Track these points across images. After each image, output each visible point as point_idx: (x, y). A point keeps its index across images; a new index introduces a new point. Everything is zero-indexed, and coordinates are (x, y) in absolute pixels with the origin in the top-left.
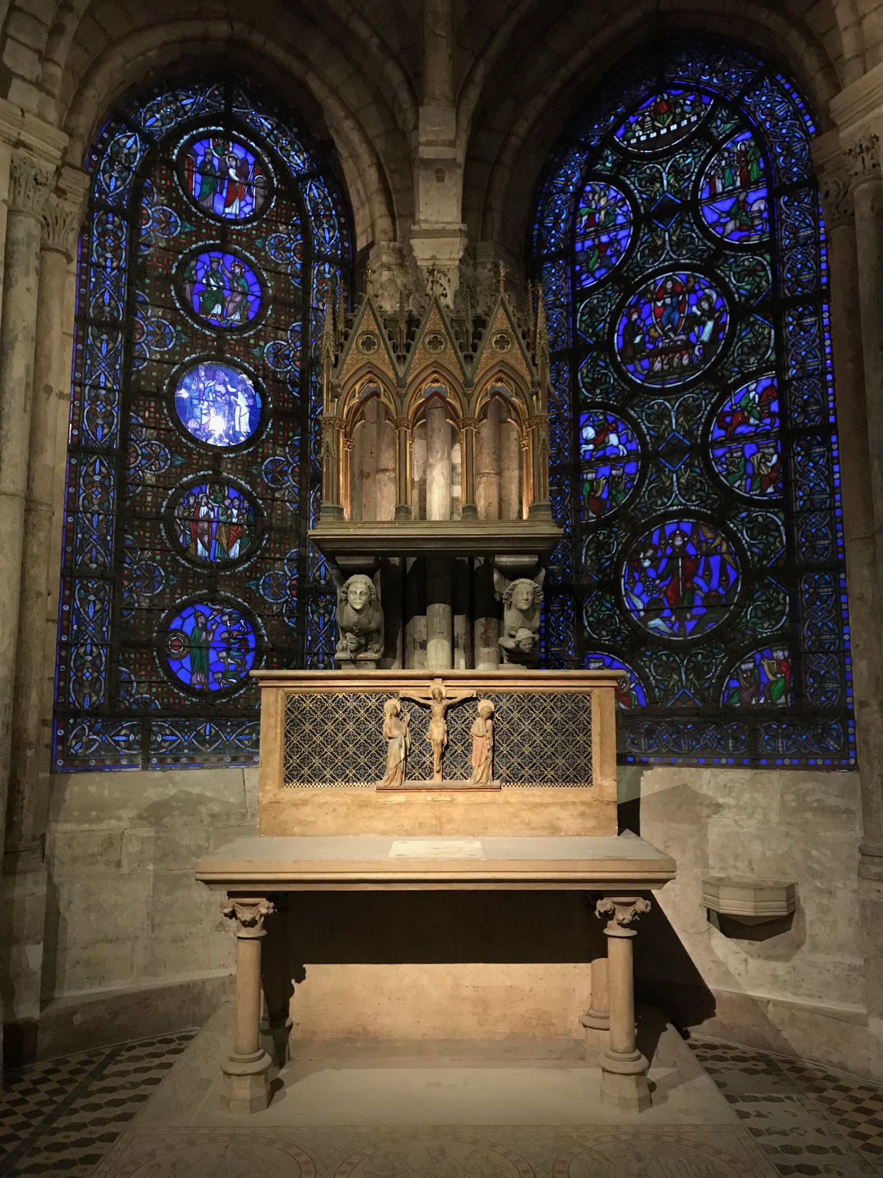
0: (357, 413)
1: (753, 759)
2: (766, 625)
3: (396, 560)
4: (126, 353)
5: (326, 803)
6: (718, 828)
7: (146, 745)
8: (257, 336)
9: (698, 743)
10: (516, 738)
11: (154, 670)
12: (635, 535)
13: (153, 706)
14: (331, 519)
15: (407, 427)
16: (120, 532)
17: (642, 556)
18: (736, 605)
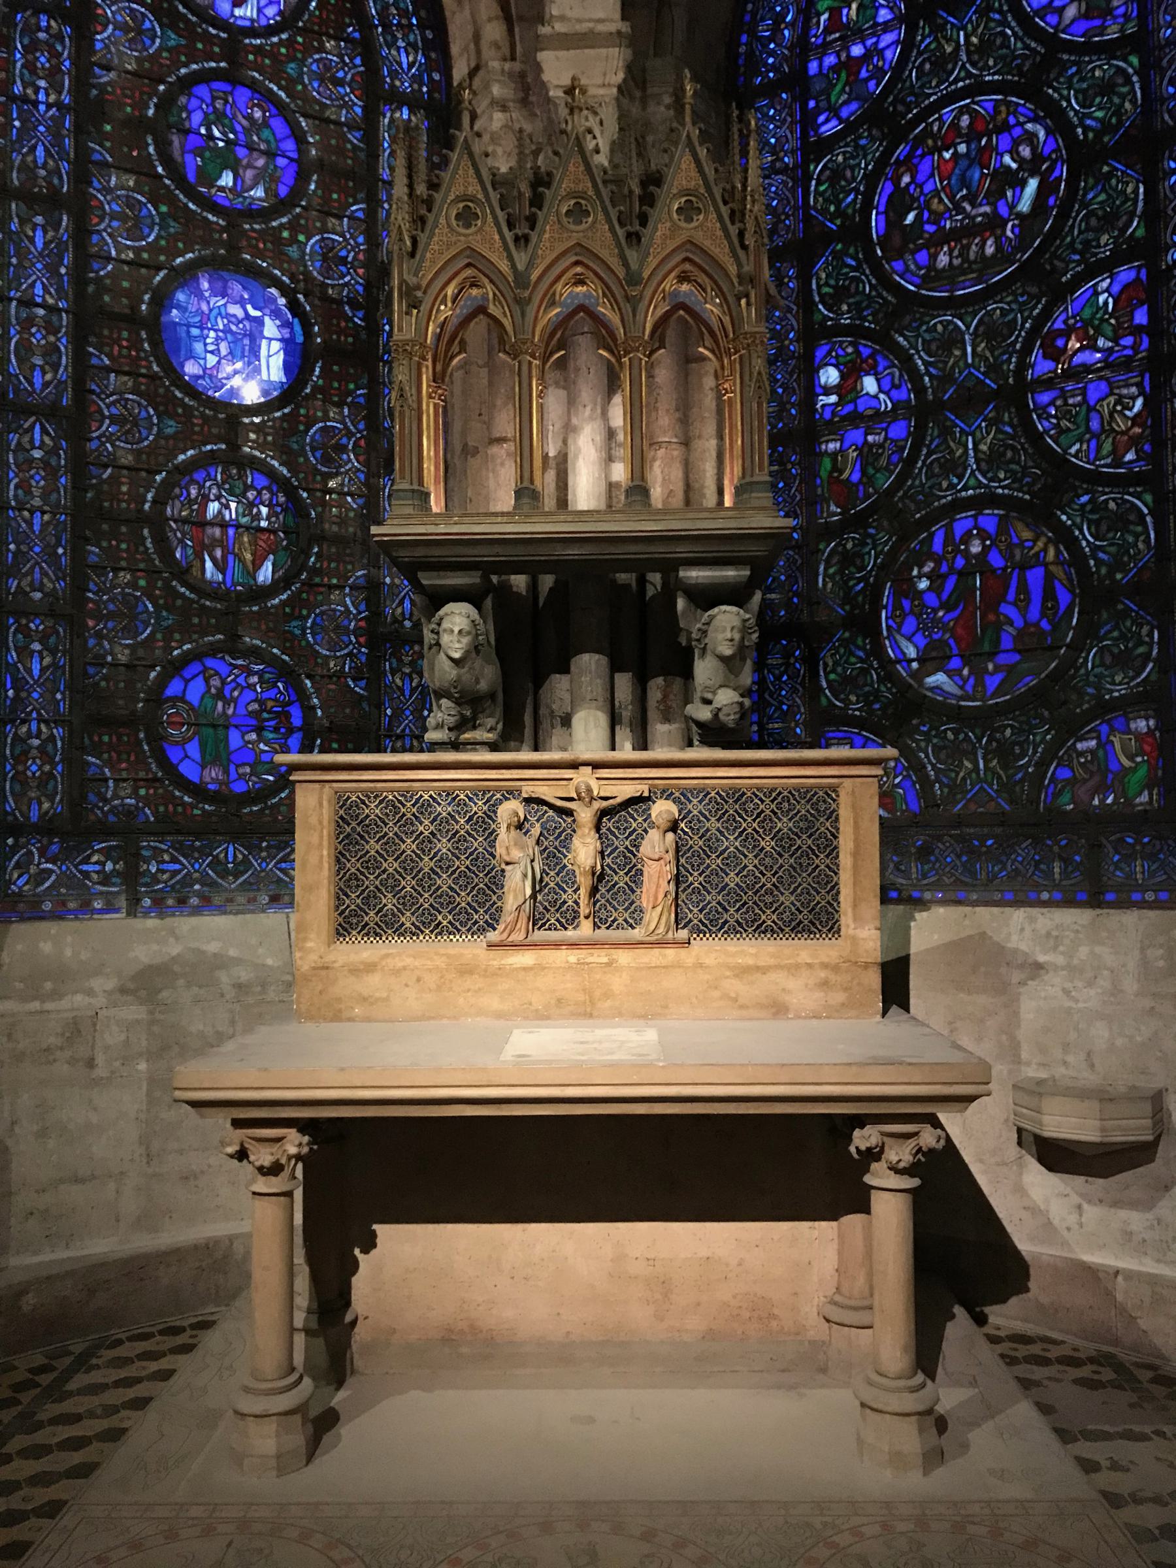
0: (452, 339)
1: (1094, 893)
2: (1118, 679)
3: (519, 581)
4: (76, 247)
5: (405, 968)
6: (1035, 1003)
7: (132, 878)
8: (293, 227)
9: (1004, 868)
10: (715, 862)
11: (141, 761)
12: (904, 539)
13: (142, 818)
14: (409, 510)
15: (533, 356)
16: (78, 543)
17: (915, 572)
18: (1068, 646)
